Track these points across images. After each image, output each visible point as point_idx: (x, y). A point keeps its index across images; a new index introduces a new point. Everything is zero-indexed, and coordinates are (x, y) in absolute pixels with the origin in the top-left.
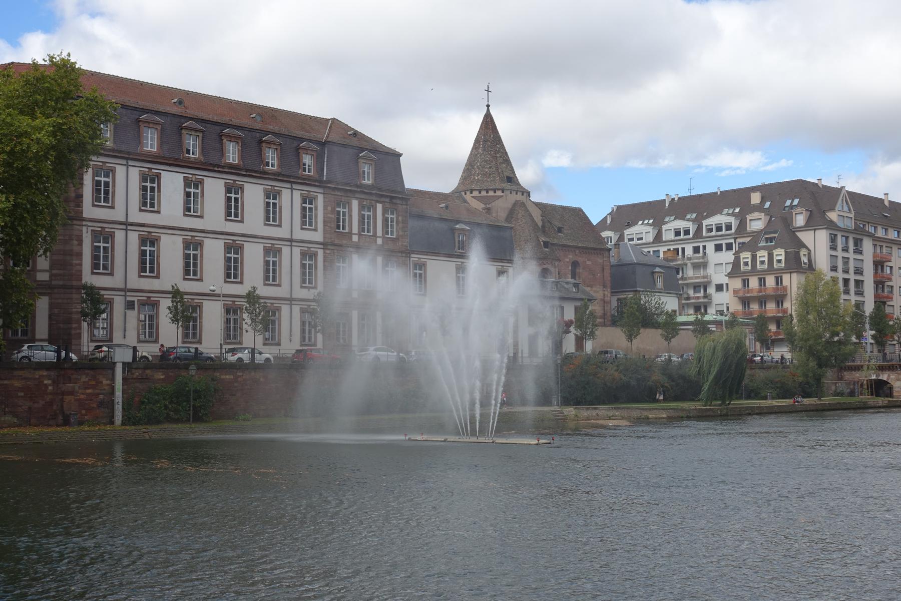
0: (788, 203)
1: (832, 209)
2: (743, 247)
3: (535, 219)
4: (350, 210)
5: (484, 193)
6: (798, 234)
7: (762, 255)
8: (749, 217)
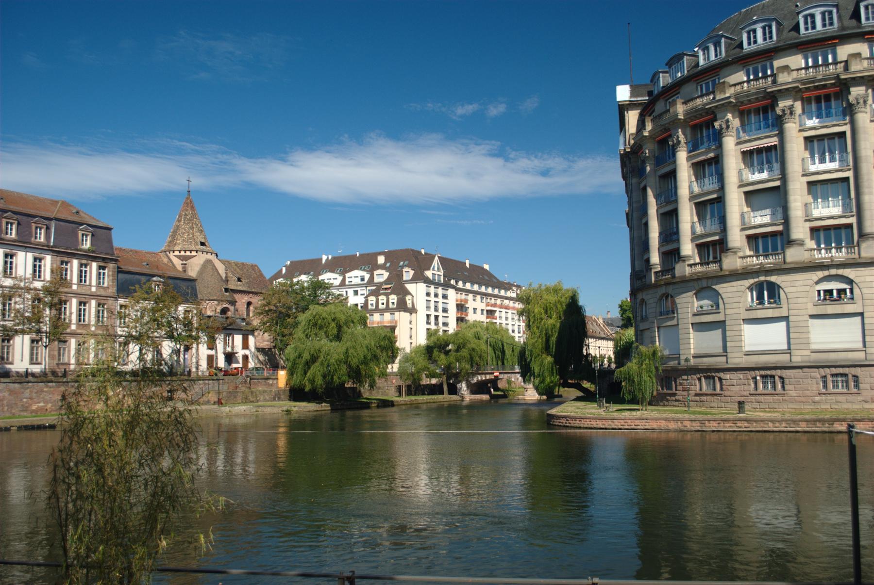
0: (402, 263)
1: (429, 269)
2: (372, 293)
3: (220, 272)
4: (72, 267)
5: (183, 253)
6: (406, 285)
7: (382, 299)
8: (376, 273)
